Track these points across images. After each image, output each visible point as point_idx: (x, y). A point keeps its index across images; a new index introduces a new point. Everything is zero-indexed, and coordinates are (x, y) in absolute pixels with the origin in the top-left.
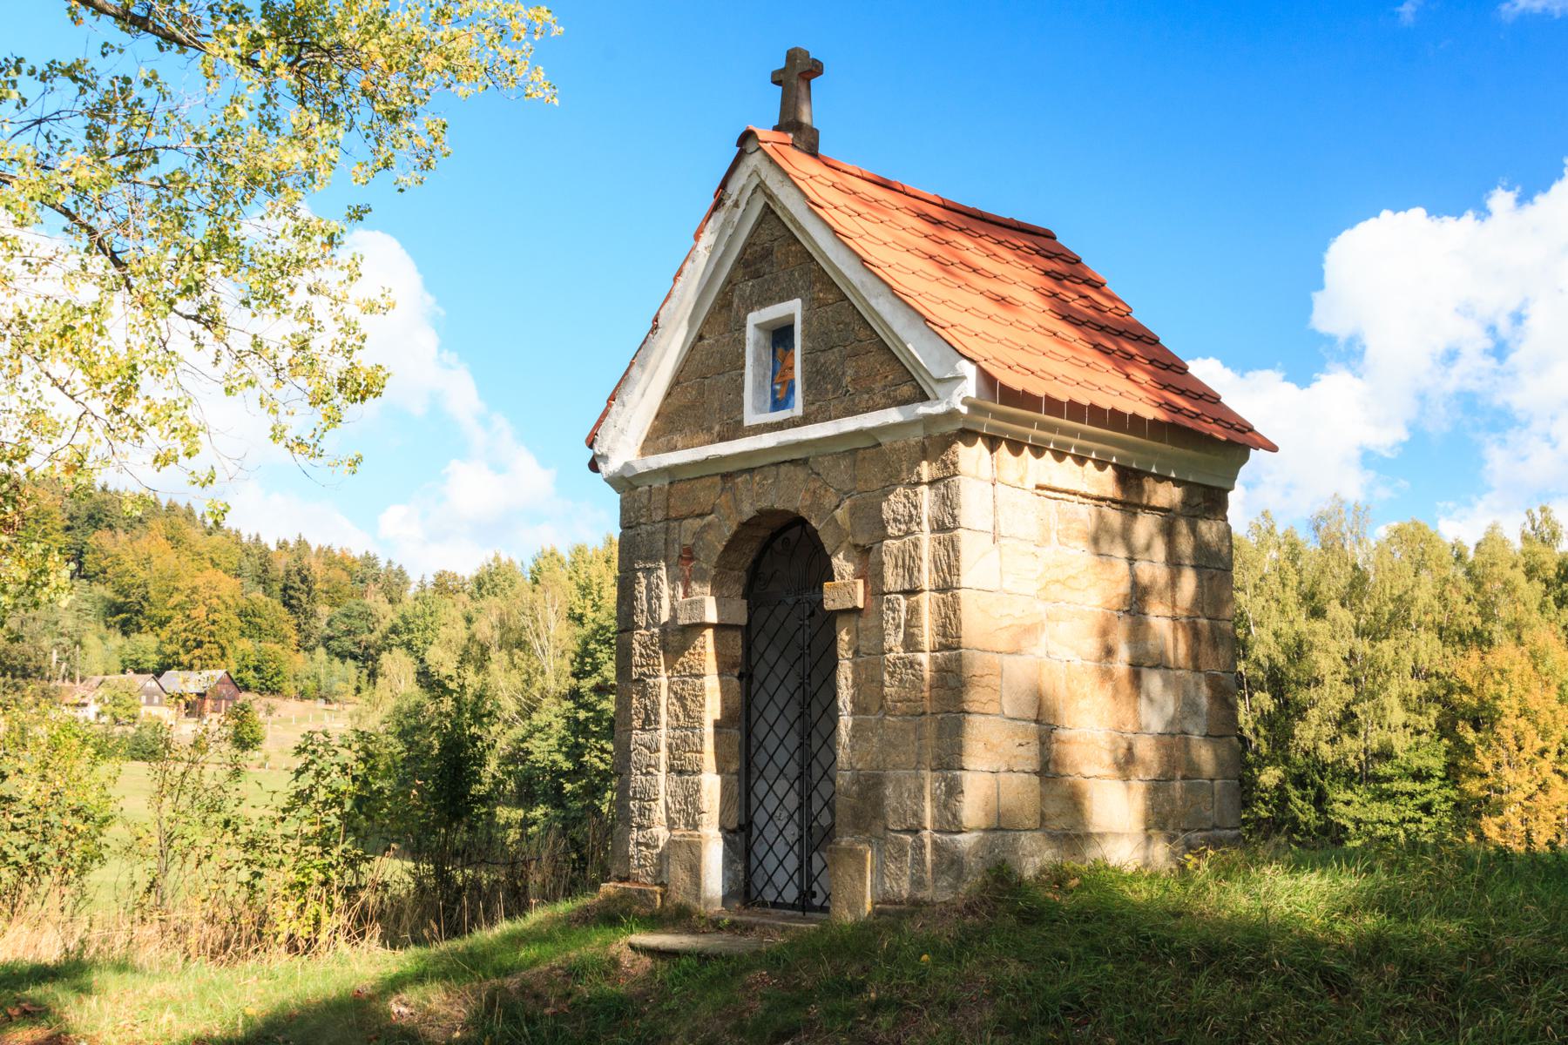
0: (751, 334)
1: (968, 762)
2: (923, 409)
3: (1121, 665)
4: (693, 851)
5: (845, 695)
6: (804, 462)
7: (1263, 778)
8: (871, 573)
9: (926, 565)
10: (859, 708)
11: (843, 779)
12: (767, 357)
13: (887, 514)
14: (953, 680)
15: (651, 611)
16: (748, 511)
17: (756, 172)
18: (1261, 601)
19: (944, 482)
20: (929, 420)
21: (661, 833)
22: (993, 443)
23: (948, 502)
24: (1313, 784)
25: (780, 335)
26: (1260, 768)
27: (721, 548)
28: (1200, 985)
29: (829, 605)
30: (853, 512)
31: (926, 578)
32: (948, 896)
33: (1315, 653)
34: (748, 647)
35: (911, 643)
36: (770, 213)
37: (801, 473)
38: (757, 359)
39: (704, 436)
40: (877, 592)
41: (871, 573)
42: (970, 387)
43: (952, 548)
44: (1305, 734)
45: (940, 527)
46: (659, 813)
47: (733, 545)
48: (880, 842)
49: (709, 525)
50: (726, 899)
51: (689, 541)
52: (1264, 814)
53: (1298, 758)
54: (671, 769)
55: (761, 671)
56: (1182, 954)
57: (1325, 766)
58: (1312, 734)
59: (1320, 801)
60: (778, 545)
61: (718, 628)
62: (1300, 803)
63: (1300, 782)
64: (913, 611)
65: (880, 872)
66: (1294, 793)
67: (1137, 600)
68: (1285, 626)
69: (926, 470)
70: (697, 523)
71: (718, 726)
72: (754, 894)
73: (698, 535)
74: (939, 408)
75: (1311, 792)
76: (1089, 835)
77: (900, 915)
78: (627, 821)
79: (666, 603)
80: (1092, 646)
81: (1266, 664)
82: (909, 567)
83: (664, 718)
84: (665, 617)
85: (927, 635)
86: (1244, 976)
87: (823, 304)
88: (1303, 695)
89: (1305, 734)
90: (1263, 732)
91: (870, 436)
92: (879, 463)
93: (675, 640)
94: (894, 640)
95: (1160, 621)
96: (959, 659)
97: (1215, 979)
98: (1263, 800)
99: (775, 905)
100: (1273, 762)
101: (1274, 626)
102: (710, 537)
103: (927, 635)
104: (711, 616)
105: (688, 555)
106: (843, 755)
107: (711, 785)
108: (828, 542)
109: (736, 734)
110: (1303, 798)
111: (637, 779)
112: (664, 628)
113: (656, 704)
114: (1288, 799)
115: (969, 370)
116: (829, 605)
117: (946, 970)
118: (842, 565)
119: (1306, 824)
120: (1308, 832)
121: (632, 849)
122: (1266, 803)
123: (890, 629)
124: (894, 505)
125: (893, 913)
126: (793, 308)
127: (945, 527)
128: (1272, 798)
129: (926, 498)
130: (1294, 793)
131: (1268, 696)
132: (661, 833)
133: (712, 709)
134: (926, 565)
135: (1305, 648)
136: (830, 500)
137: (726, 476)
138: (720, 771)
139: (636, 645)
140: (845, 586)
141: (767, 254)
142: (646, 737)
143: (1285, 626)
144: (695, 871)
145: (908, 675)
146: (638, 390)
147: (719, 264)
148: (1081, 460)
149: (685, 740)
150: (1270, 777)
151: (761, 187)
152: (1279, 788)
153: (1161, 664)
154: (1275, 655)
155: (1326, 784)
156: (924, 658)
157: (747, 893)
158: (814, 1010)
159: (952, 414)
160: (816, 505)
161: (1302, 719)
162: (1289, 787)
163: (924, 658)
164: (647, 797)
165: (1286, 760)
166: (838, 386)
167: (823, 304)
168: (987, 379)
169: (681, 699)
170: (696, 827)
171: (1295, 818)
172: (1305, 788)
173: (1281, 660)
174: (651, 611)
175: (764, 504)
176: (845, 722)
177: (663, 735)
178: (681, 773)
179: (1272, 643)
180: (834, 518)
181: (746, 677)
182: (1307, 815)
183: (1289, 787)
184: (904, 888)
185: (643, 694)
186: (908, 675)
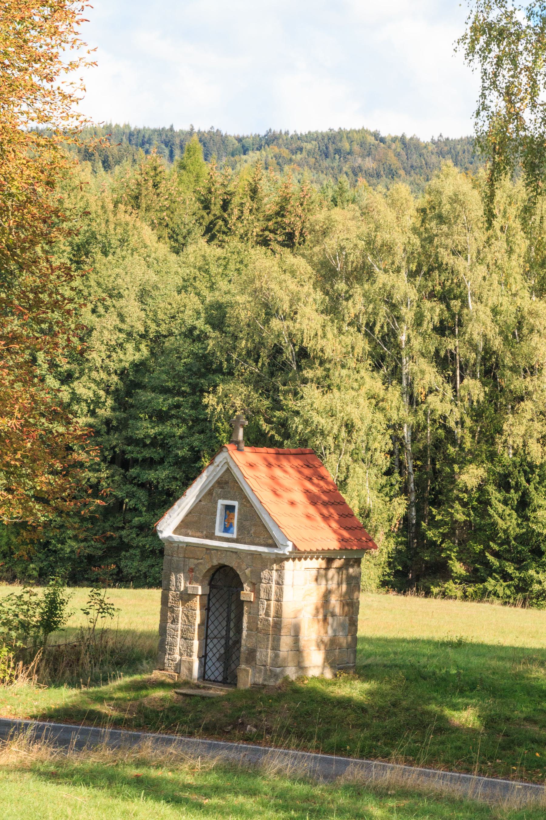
0: (219, 507)
1: (281, 649)
2: (276, 551)
3: (321, 617)
4: (191, 663)
5: (245, 625)
6: (236, 553)
7: (464, 478)
8: (256, 591)
9: (273, 593)
10: (249, 629)
11: (243, 649)
12: (224, 513)
13: (262, 576)
14: (278, 626)
15: (177, 586)
16: (215, 563)
17: (226, 458)
18: (481, 270)
19: (280, 571)
20: (277, 554)
21: (177, 657)
22: (294, 559)
23: (281, 577)
24: (517, 487)
25: (229, 509)
26: (463, 463)
27: (204, 571)
28: (335, 710)
29: (242, 598)
30: (252, 572)
31: (273, 597)
32: (273, 684)
33: (535, 338)
34: (209, 600)
35: (267, 614)
36: (228, 470)
37: (234, 556)
38: (221, 515)
39: (199, 534)
40: (257, 596)
41: (256, 591)
42: (290, 548)
43: (281, 590)
44: (515, 430)
45: (278, 583)
46: (177, 650)
47: (208, 570)
48: (254, 667)
49: (201, 563)
50: (198, 679)
51: (193, 567)
52: (460, 517)
53: (508, 457)
54: (182, 637)
55: (213, 609)
56: (332, 703)
57: (532, 466)
58: (521, 430)
59: (523, 505)
60: (222, 570)
61: (201, 596)
62: (500, 507)
63: (504, 483)
64: (269, 606)
65: (254, 676)
66: (495, 495)
67: (327, 594)
68: (505, 301)
69: (275, 566)
70: (196, 562)
71: (199, 625)
72: (206, 677)
73: (197, 565)
74: (281, 552)
75: (514, 496)
76: (306, 668)
77: (260, 688)
78: (164, 652)
79: (183, 584)
80: (314, 612)
81: (481, 345)
82: (268, 593)
83: (180, 621)
84: (182, 589)
85: (272, 613)
86: (345, 708)
87: (245, 506)
88: (518, 383)
89: (515, 430)
90: (468, 422)
91: (260, 554)
92: (264, 562)
93: (186, 597)
94: (262, 613)
95: (334, 601)
96: (281, 621)
97: (339, 709)
98: (460, 500)
99: (214, 681)
100: (475, 457)
101: (492, 300)
102: (201, 567)
103: (272, 613)
104: (200, 592)
105: (192, 570)
106: (243, 642)
107: (196, 643)
108: (243, 580)
109: (204, 628)
110: (505, 502)
111: (169, 639)
112: (181, 593)
113: (177, 616)
114: (488, 503)
115: (290, 544)
116: (242, 598)
117: (276, 704)
118: (247, 587)
119: (505, 531)
120: (506, 541)
121: (166, 661)
122: (465, 505)
123: (261, 609)
124: (265, 574)
125: (257, 688)
126: (235, 503)
127: (280, 584)
128: (471, 499)
129: (274, 574)
130: (495, 495)
131: (479, 384)
132: (177, 657)
133: (198, 621)
134: (273, 593)
135: (525, 331)
136: (244, 566)
137: (207, 549)
138: (199, 639)
139: (171, 597)
140: (247, 594)
141: (227, 483)
142: (173, 626)
143: (505, 301)
144: (190, 670)
145: (266, 623)
146: (176, 513)
147: (210, 482)
148: (317, 559)
149: (188, 629)
150: (471, 476)
151: (227, 463)
152: (480, 488)
153: (333, 615)
154: (490, 335)
155: (531, 488)
156: (271, 619)
157: (204, 677)
158: (243, 712)
159: (284, 554)
160: (239, 566)
161: (514, 411)
162: (491, 488)
163: (271, 619)
164: (172, 645)
165: (492, 456)
166: (249, 533)
167: (245, 506)
168: (295, 546)
169: (187, 616)
170: (191, 656)
171: (494, 524)
172: (508, 492)
173: (497, 343)
174: (177, 586)
175: (222, 562)
176: (245, 633)
177: (180, 626)
178: (185, 639)
179: (488, 322)
180: (245, 572)
181: (208, 609)
182: (507, 522)
183: (491, 488)
184: (260, 681)
185: (173, 612)
186: (266, 623)
